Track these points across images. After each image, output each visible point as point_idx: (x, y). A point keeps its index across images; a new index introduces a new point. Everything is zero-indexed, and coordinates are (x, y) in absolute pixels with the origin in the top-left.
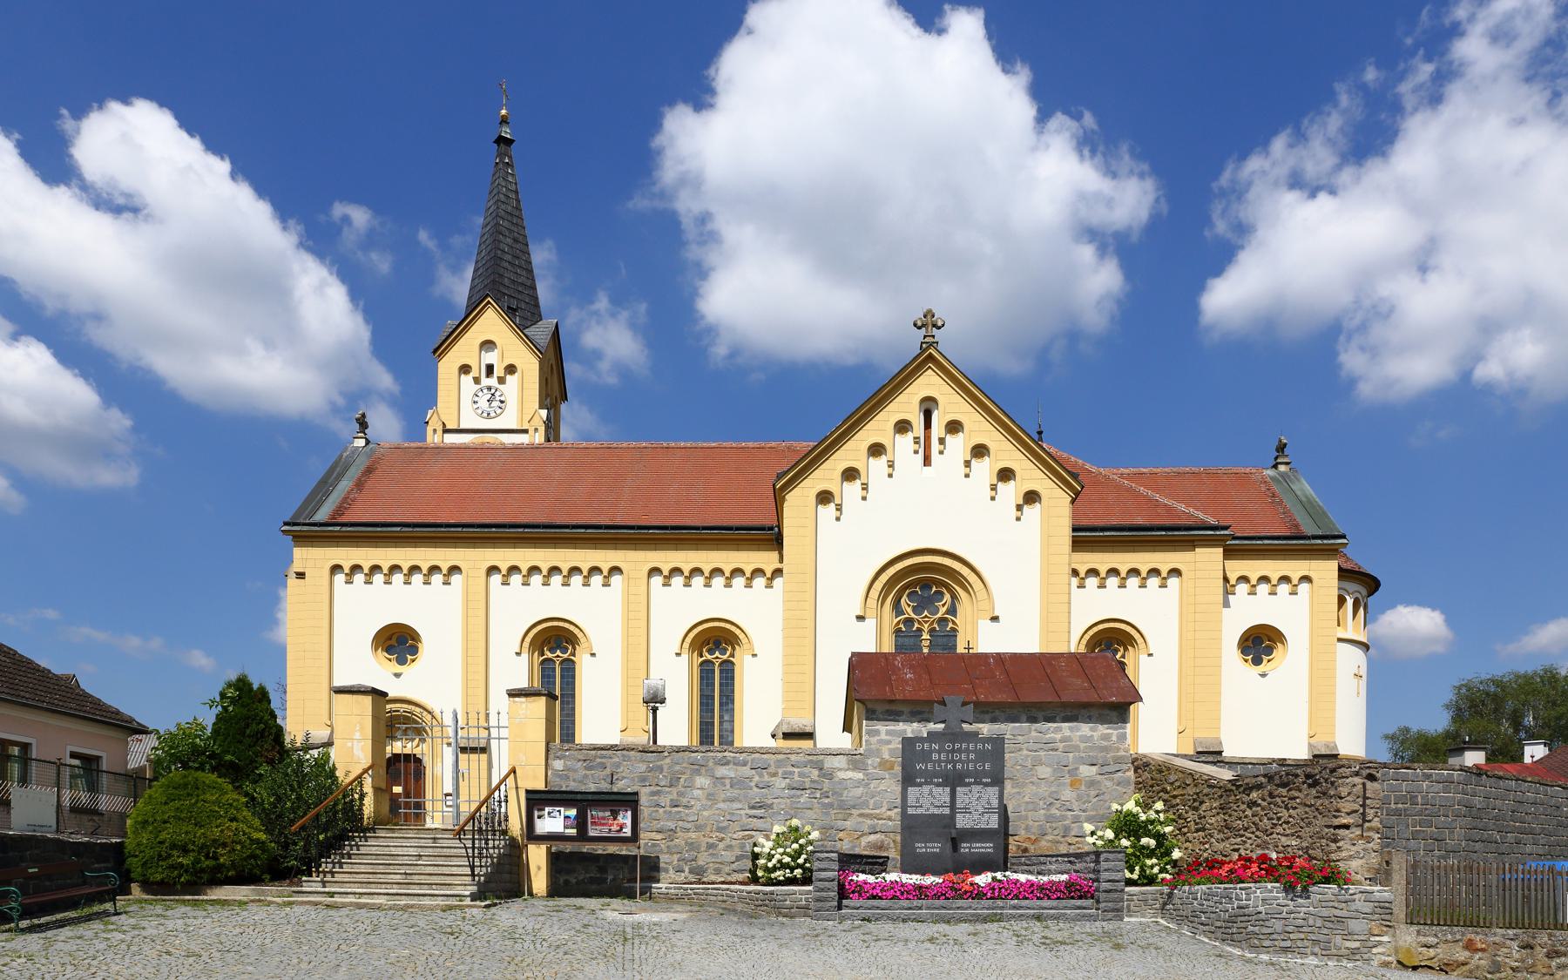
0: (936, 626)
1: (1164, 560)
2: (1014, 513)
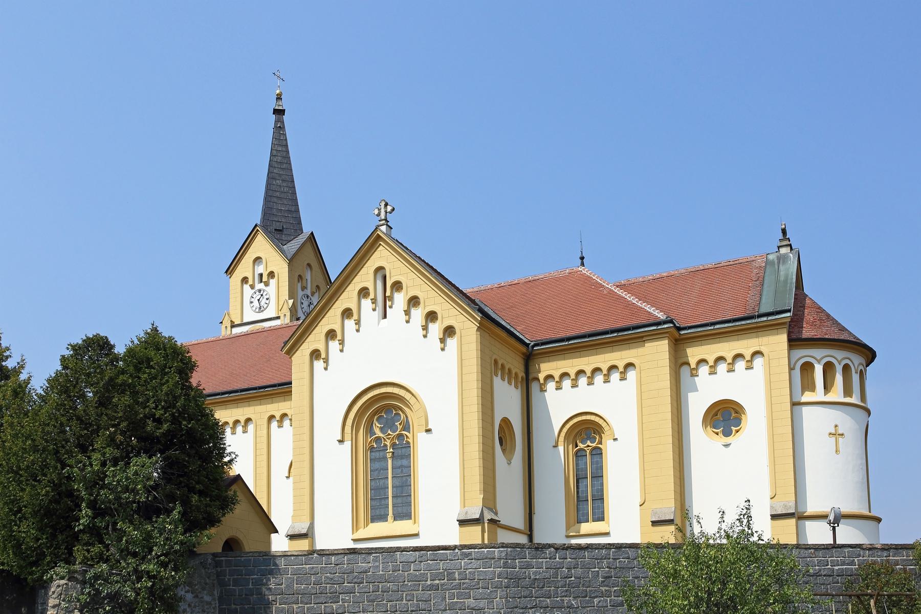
0: (374, 444)
1: (619, 357)
2: (439, 345)
